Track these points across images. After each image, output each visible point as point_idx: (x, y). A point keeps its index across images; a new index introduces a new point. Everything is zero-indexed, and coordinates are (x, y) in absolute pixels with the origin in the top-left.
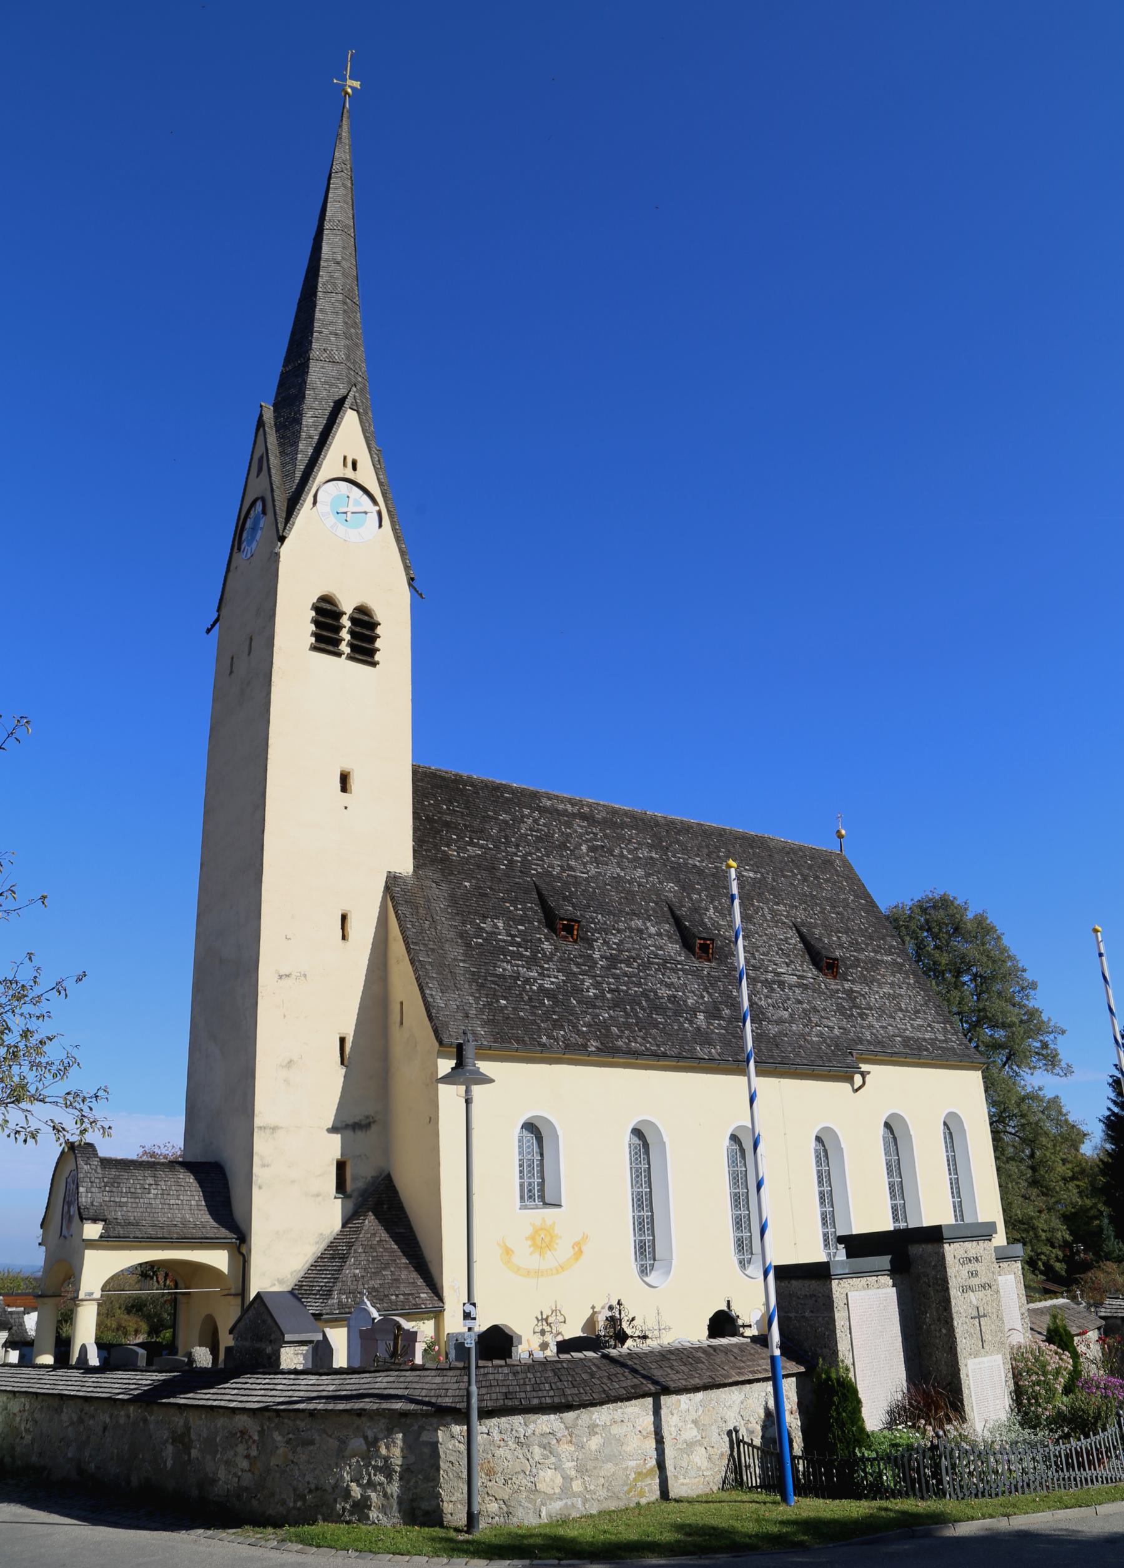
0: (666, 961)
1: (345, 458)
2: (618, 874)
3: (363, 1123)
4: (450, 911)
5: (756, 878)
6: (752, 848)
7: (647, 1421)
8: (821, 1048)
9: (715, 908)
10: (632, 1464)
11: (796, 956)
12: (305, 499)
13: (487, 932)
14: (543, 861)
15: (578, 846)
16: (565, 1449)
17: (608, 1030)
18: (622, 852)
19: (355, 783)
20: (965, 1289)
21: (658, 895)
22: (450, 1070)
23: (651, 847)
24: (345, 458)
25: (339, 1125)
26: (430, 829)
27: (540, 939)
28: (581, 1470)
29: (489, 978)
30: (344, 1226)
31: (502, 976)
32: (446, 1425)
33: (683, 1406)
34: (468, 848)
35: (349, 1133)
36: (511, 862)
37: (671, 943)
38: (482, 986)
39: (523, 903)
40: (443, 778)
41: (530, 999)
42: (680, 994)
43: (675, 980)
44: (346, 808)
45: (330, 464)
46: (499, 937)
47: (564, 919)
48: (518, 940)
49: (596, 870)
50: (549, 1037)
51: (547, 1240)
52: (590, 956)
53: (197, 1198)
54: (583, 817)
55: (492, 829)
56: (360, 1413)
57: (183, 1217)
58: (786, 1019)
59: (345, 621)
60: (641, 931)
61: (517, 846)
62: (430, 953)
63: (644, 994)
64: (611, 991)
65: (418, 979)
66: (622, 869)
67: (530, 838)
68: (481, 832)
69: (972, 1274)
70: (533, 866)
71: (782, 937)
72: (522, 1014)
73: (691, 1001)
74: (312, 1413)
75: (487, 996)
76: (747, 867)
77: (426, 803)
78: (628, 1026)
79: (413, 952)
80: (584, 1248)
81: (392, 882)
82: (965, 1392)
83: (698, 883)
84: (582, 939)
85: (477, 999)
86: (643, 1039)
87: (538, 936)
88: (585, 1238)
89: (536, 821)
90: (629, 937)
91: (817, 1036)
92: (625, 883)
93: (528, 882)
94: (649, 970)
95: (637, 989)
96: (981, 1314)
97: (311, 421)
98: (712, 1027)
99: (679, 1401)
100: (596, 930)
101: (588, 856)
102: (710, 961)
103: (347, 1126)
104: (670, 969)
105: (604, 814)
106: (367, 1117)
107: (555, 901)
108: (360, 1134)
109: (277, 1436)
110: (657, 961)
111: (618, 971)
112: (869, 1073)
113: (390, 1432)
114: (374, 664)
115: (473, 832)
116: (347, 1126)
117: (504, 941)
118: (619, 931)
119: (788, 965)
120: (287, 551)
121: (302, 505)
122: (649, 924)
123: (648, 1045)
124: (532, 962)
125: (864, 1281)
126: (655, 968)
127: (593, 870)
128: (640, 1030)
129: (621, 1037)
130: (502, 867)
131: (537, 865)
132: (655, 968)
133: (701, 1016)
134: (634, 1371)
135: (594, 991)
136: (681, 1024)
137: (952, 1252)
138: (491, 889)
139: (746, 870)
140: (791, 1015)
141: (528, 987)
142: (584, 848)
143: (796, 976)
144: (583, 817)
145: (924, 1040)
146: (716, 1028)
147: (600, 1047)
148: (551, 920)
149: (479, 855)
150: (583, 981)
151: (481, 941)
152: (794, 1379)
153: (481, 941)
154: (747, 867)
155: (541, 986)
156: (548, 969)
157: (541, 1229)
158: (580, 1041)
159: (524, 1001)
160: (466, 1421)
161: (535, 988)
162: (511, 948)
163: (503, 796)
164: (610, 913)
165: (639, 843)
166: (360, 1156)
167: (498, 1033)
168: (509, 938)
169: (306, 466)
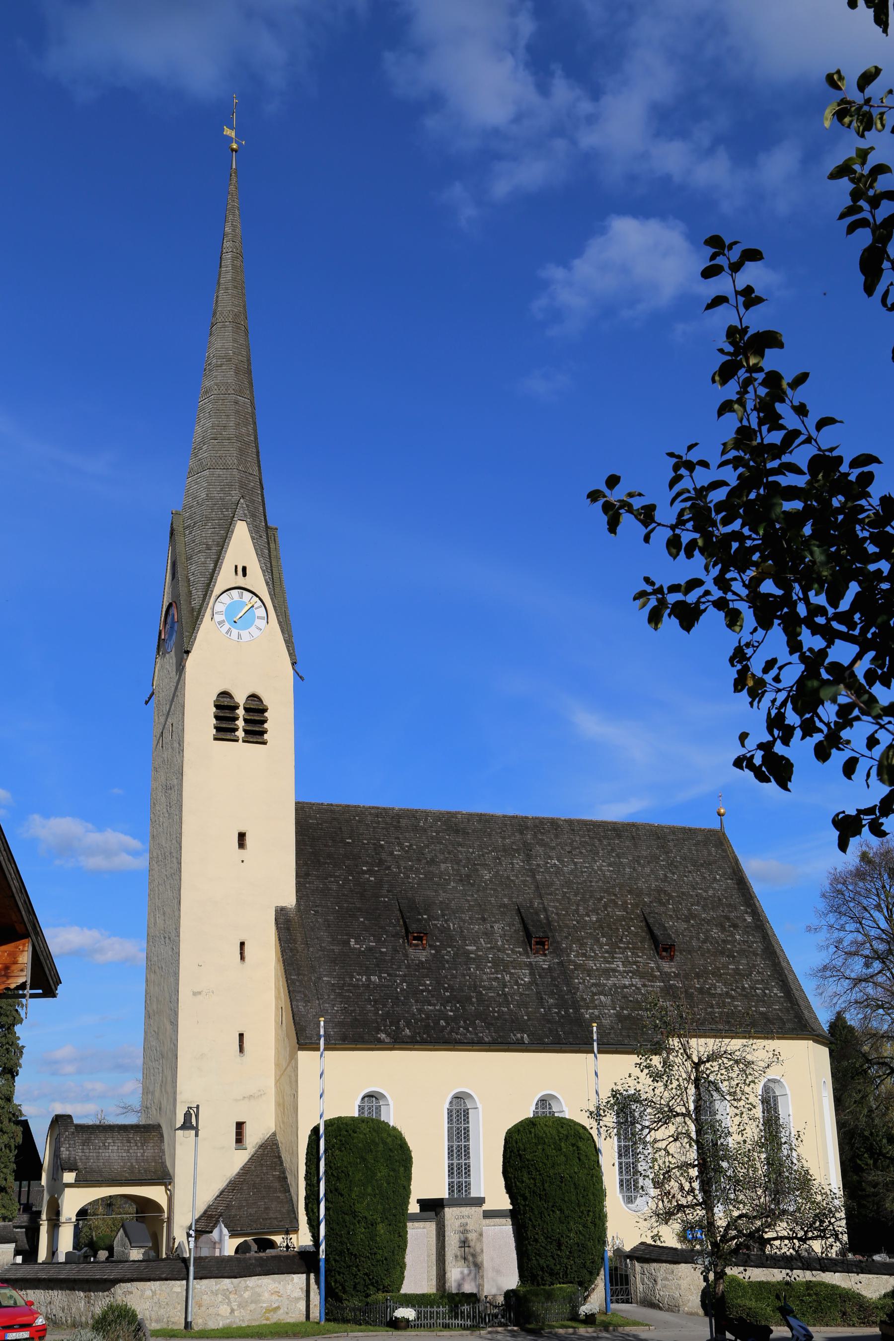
1: (236, 567)
10: (265, 1305)
16: (232, 1296)
24: (236, 567)
28: (240, 1306)
31: (356, 986)
44: (243, 861)
45: (225, 577)
53: (485, 977)
57: (132, 1164)
59: (241, 712)
99: (292, 1280)
160: (47, 1261)
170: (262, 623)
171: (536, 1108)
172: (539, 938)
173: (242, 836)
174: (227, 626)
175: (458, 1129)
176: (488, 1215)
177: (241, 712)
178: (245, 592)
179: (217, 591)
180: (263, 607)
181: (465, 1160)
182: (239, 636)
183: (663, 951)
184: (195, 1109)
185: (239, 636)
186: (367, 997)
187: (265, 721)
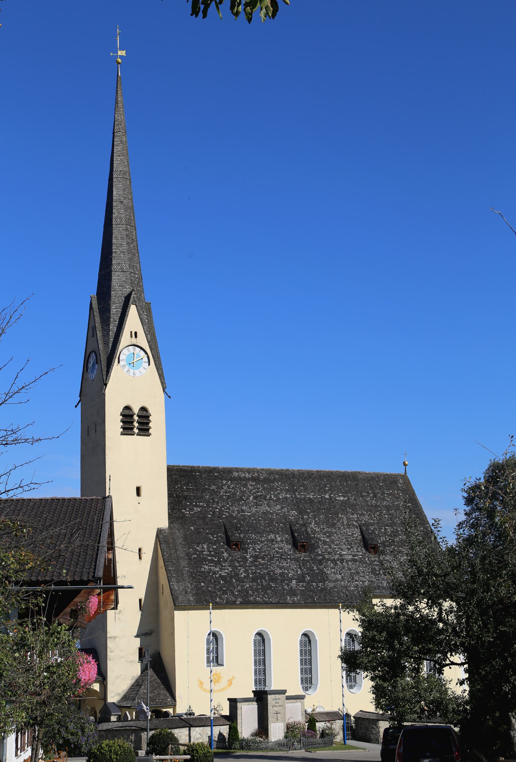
1: (131, 332)
2: (267, 510)
3: (149, 633)
4: (183, 543)
6: (347, 481)
7: (187, 732)
8: (354, 593)
9: (316, 522)
11: (355, 544)
12: (114, 361)
13: (199, 551)
14: (230, 509)
15: (248, 498)
17: (247, 592)
18: (271, 497)
19: (143, 492)
20: (273, 706)
21: (285, 519)
23: (287, 491)
24: (131, 332)
25: (139, 634)
26: (178, 501)
27: (223, 551)
29: (198, 574)
30: (142, 673)
32: (144, 732)
33: (197, 730)
34: (194, 508)
35: (143, 637)
36: (214, 512)
37: (287, 545)
38: (194, 578)
39: (217, 534)
40: (185, 471)
41: (215, 582)
42: (286, 571)
43: (285, 564)
44: (139, 503)
45: (125, 339)
46: (204, 553)
47: (234, 542)
48: (213, 553)
49: (256, 510)
50: (220, 599)
52: (245, 557)
54: (253, 479)
55: (206, 496)
56: (126, 730)
58: (339, 579)
59: (136, 418)
60: (272, 540)
61: (218, 503)
62: (173, 565)
63: (268, 573)
64: (252, 573)
65: (168, 577)
66: (269, 507)
67: (225, 497)
68: (201, 498)
70: (224, 513)
71: (350, 534)
72: (210, 589)
73: (291, 574)
74: (116, 730)
75: (196, 582)
76: (340, 494)
77: (176, 487)
78: (257, 590)
79: (166, 566)
80: (232, 682)
81: (160, 532)
82: (269, 731)
83: (309, 509)
84: (243, 549)
85: (191, 584)
86: (263, 595)
87: (222, 550)
88: (233, 678)
89: (229, 487)
90: (266, 544)
91: (354, 587)
92: (269, 515)
93: (221, 522)
94: (273, 561)
95: (265, 571)
97: (115, 310)
98: (298, 587)
100: (250, 543)
101: (252, 502)
103: (143, 635)
104: (283, 559)
105: (265, 476)
106: (151, 630)
107: (231, 532)
108: (148, 637)
109: (109, 736)
110: (278, 555)
113: (132, 734)
114: (149, 435)
115: (198, 499)
116: (143, 635)
117: (206, 555)
118: (261, 542)
119: (349, 549)
120: (108, 391)
121: (113, 365)
122: (277, 536)
123: (264, 598)
124: (218, 563)
125: (248, 703)
126: (276, 559)
127: (254, 510)
128: (262, 591)
129: (252, 596)
130: (209, 516)
131: (226, 512)
132: (276, 559)
133: (294, 582)
134: (186, 722)
135: (244, 574)
136: (283, 586)
137: (270, 697)
138: (203, 529)
139: (339, 496)
140: (342, 577)
143: (352, 555)
144: (253, 479)
146: (300, 587)
147: (242, 601)
148: (229, 542)
149: (199, 511)
150: (240, 570)
151: (196, 556)
152: (111, 721)
153: (196, 556)
154: (340, 494)
155: (220, 574)
156: (224, 566)
158: (233, 599)
159: (212, 583)
161: (217, 576)
162: (209, 558)
163: (213, 475)
164: (259, 533)
165: (281, 490)
167: (199, 599)
168: (209, 553)
169: (114, 339)
171: (301, 638)
172: (302, 543)
173: (138, 489)
175: (259, 650)
176: (289, 698)
177: (136, 418)
178: (137, 348)
179: (121, 347)
182: (134, 374)
183: (371, 549)
185: (134, 374)
186: (209, 579)
187: (148, 423)
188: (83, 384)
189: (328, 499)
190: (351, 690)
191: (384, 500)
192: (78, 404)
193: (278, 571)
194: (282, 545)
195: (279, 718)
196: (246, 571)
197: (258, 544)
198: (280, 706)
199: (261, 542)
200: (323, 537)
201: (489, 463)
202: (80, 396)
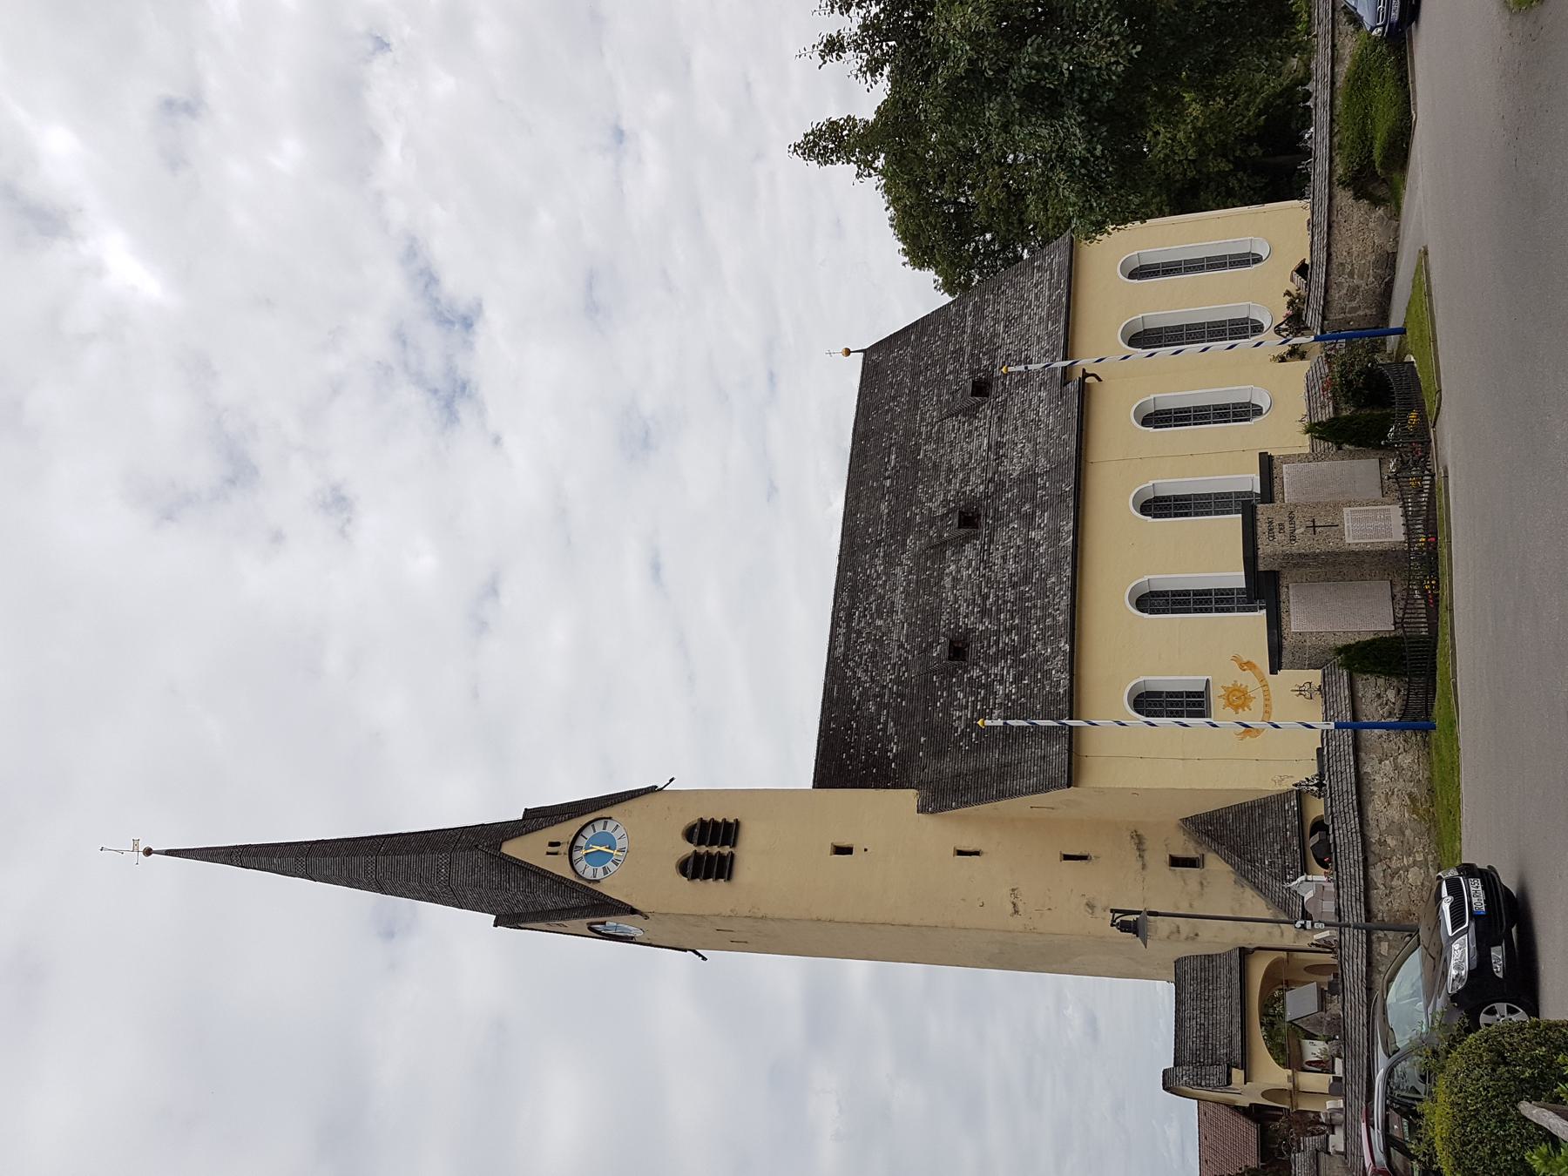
0: (982, 561)
1: (548, 853)
2: (902, 593)
3: (1137, 841)
5: (896, 453)
16: (1395, 864)
19: (844, 842)
20: (1293, 538)
22: (1138, 939)
24: (548, 853)
45: (559, 867)
51: (1238, 694)
59: (703, 849)
64: (1013, 618)
69: (1281, 529)
77: (850, 768)
80: (1245, 660)
88: (1236, 659)
96: (1318, 530)
98: (1042, 525)
102: (979, 516)
106: (1132, 837)
108: (1148, 844)
111: (994, 608)
112: (1084, 370)
139: (889, 461)
141: (1013, 697)
142: (879, 622)
145: (1050, 296)
151: (974, 735)
153: (974, 735)
157: (1228, 699)
166: (1166, 845)
170: (611, 826)
174: (610, 865)
177: (703, 849)
180: (595, 823)
181: (1211, 595)
184: (1117, 915)
188: (663, 945)
189: (892, 482)
190: (1264, 412)
191: (900, 383)
192: (700, 955)
193: (1011, 566)
194: (964, 562)
195: (1329, 520)
196: (1008, 631)
197: (959, 608)
198: (1291, 519)
199: (956, 602)
200: (956, 484)
201: (909, 267)
202: (685, 950)
